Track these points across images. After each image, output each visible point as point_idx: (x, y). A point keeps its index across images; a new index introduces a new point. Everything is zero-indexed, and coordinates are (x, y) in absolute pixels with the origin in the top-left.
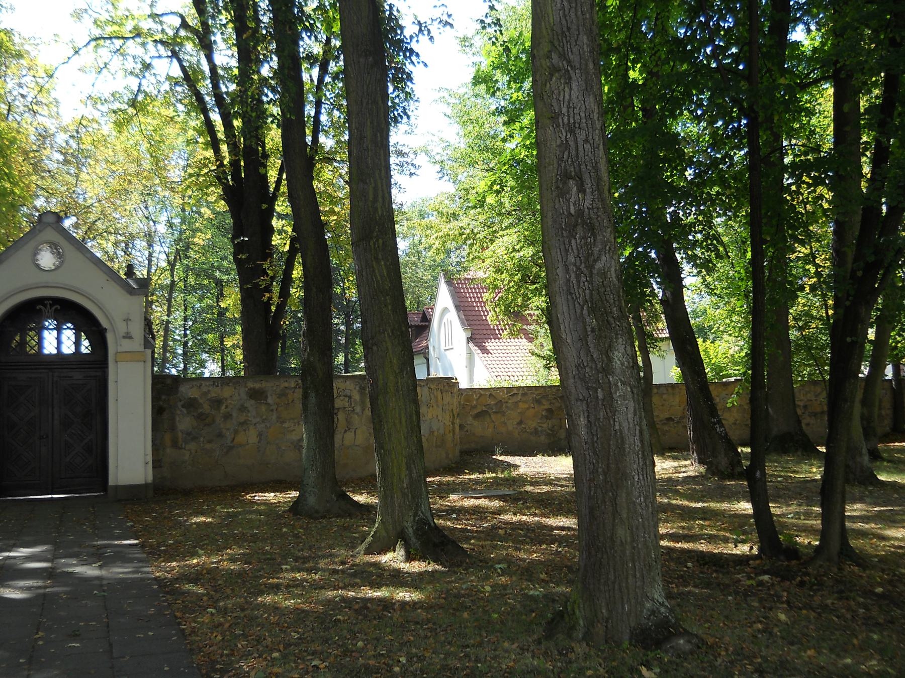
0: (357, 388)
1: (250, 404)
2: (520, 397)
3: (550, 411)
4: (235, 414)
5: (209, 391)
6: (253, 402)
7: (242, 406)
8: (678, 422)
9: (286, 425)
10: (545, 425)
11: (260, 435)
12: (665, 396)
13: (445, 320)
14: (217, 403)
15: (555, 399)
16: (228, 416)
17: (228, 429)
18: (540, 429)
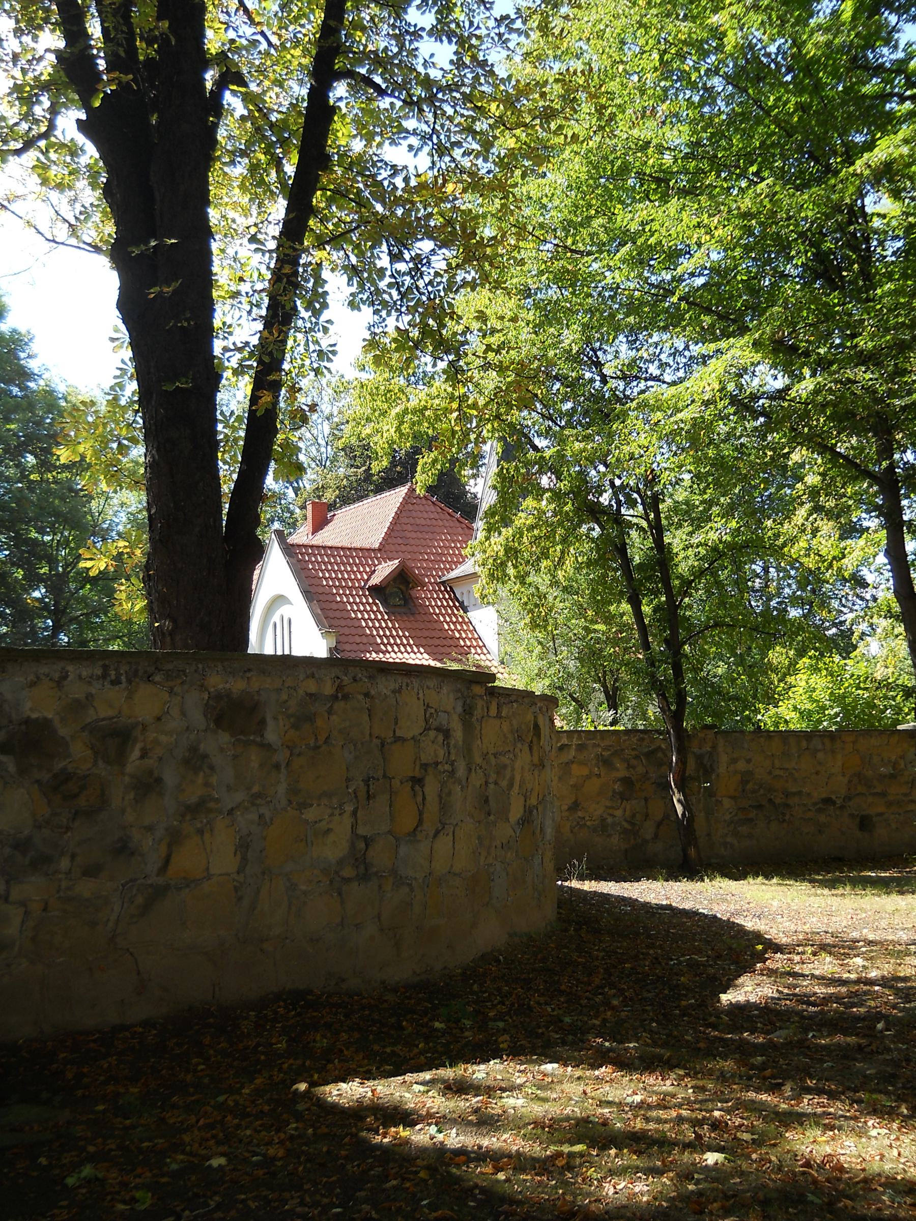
0: (459, 709)
1: (218, 744)
2: (573, 753)
3: (627, 782)
4: (170, 778)
5: (89, 697)
6: (225, 738)
7: (193, 749)
8: (842, 807)
9: (310, 814)
10: (619, 813)
11: (243, 846)
12: (820, 755)
13: (276, 618)
14: (116, 738)
15: (637, 757)
16: (147, 786)
17: (150, 829)
18: (610, 820)
